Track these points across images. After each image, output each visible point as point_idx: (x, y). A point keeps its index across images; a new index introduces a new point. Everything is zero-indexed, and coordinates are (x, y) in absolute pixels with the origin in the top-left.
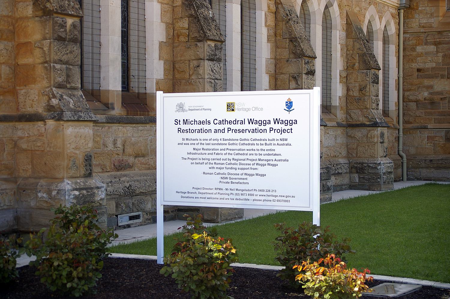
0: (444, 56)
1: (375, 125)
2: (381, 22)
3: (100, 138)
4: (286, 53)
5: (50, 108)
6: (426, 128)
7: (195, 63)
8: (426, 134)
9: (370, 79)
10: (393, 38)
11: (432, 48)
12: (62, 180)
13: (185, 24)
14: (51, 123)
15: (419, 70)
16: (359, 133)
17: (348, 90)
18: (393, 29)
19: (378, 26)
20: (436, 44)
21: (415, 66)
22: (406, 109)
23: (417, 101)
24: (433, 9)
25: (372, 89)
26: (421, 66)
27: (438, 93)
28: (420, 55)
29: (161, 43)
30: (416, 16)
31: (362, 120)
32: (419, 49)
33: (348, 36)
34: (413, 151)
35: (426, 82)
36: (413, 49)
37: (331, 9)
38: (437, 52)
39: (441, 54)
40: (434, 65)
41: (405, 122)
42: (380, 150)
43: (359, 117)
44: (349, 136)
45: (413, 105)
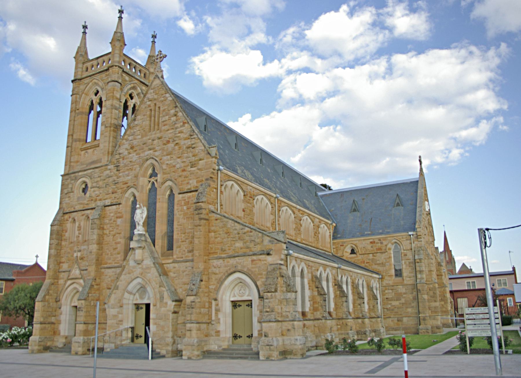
0: (395, 294)
1: (378, 317)
2: (325, 273)
3: (434, 293)
4: (356, 297)
5: (323, 317)
6: (390, 317)
7: (342, 303)
8: (391, 319)
9: (376, 303)
10: (378, 288)
11: (391, 291)
12: (327, 333)
13: (338, 292)
14: (323, 321)
15: (387, 298)
16: (373, 320)
17: (369, 306)
18: (378, 286)
19: (374, 285)
20: (392, 290)
21: (385, 297)
22: (384, 311)
23: (387, 309)
24: (390, 278)
25: (376, 306)
26: (387, 297)
27: (394, 306)
28: (387, 293)
29: (333, 298)
30: (385, 281)
31: (374, 316)
32: (386, 291)
33: (368, 290)
34: (387, 325)
35: (390, 302)
36: (384, 292)
37: (295, 268)
38: (392, 292)
39: (393, 293)
40: (391, 296)
41: (384, 316)
42: (380, 325)
43: (373, 315)
44: (371, 321)
45: (386, 310)
